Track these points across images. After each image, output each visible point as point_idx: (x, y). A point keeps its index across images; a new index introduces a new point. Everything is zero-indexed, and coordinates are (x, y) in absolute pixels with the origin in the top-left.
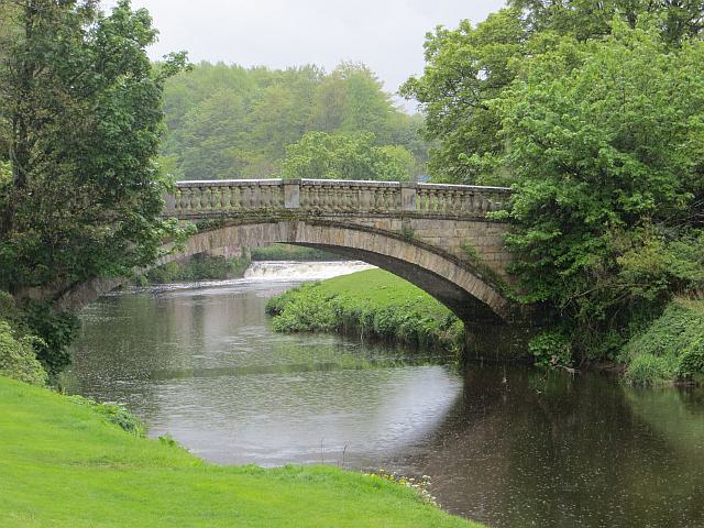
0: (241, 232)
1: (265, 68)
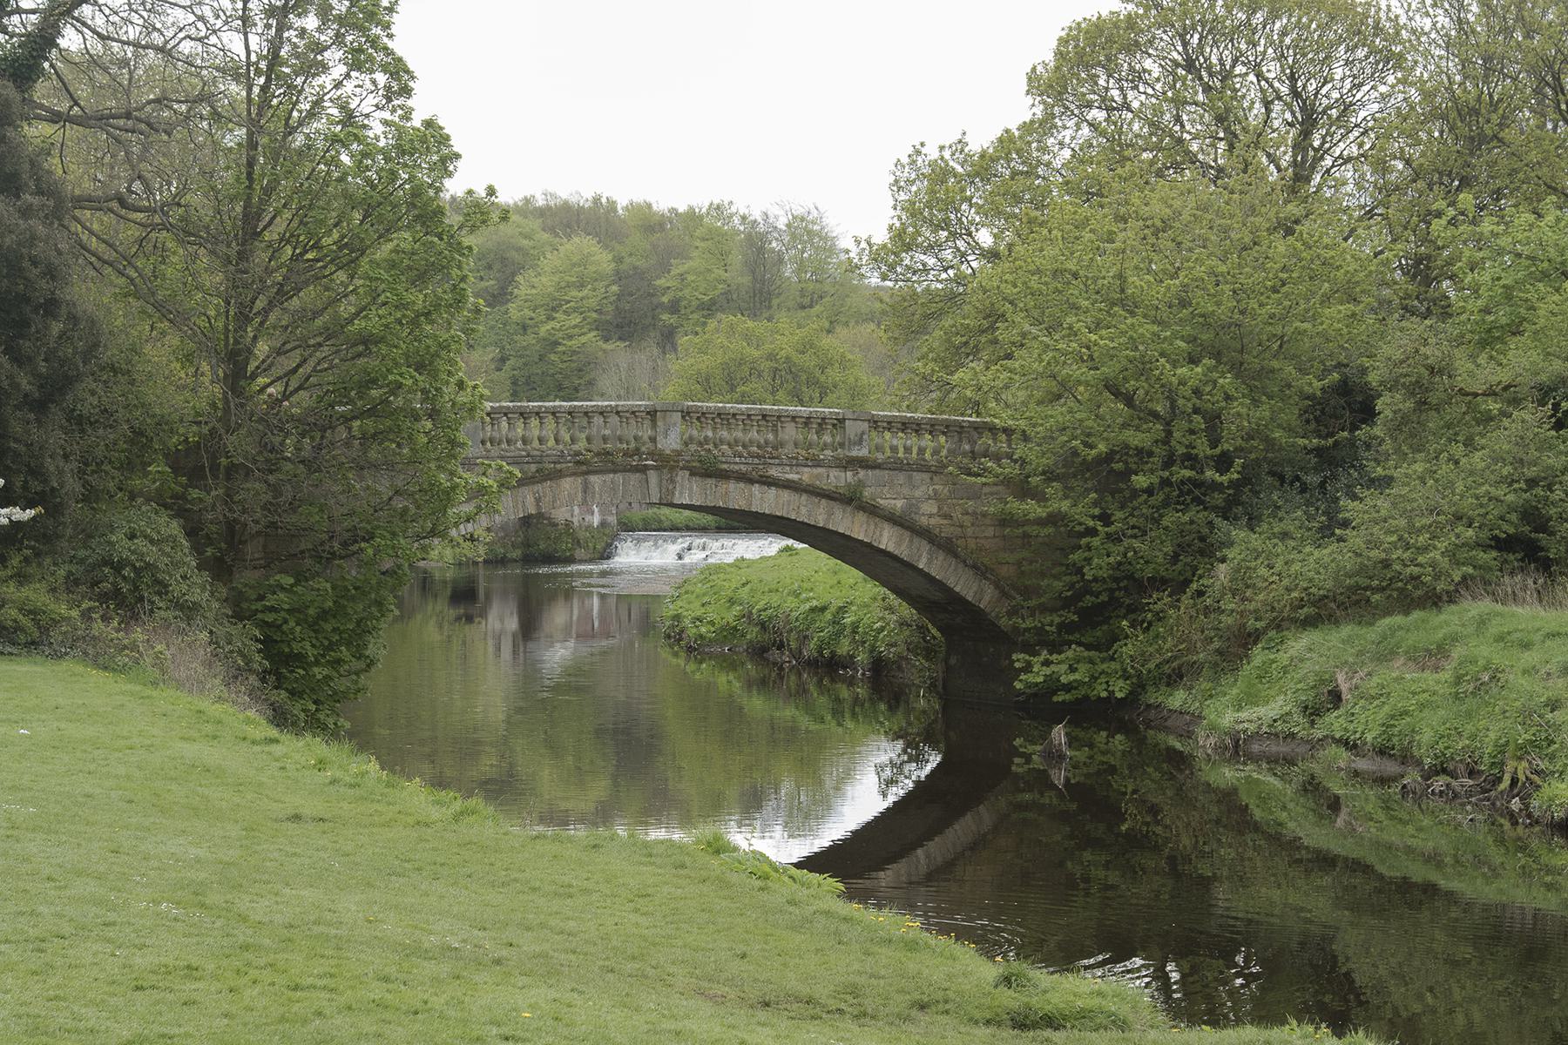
0: (586, 488)
1: (649, 206)
